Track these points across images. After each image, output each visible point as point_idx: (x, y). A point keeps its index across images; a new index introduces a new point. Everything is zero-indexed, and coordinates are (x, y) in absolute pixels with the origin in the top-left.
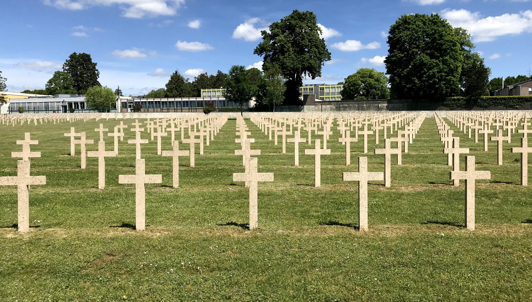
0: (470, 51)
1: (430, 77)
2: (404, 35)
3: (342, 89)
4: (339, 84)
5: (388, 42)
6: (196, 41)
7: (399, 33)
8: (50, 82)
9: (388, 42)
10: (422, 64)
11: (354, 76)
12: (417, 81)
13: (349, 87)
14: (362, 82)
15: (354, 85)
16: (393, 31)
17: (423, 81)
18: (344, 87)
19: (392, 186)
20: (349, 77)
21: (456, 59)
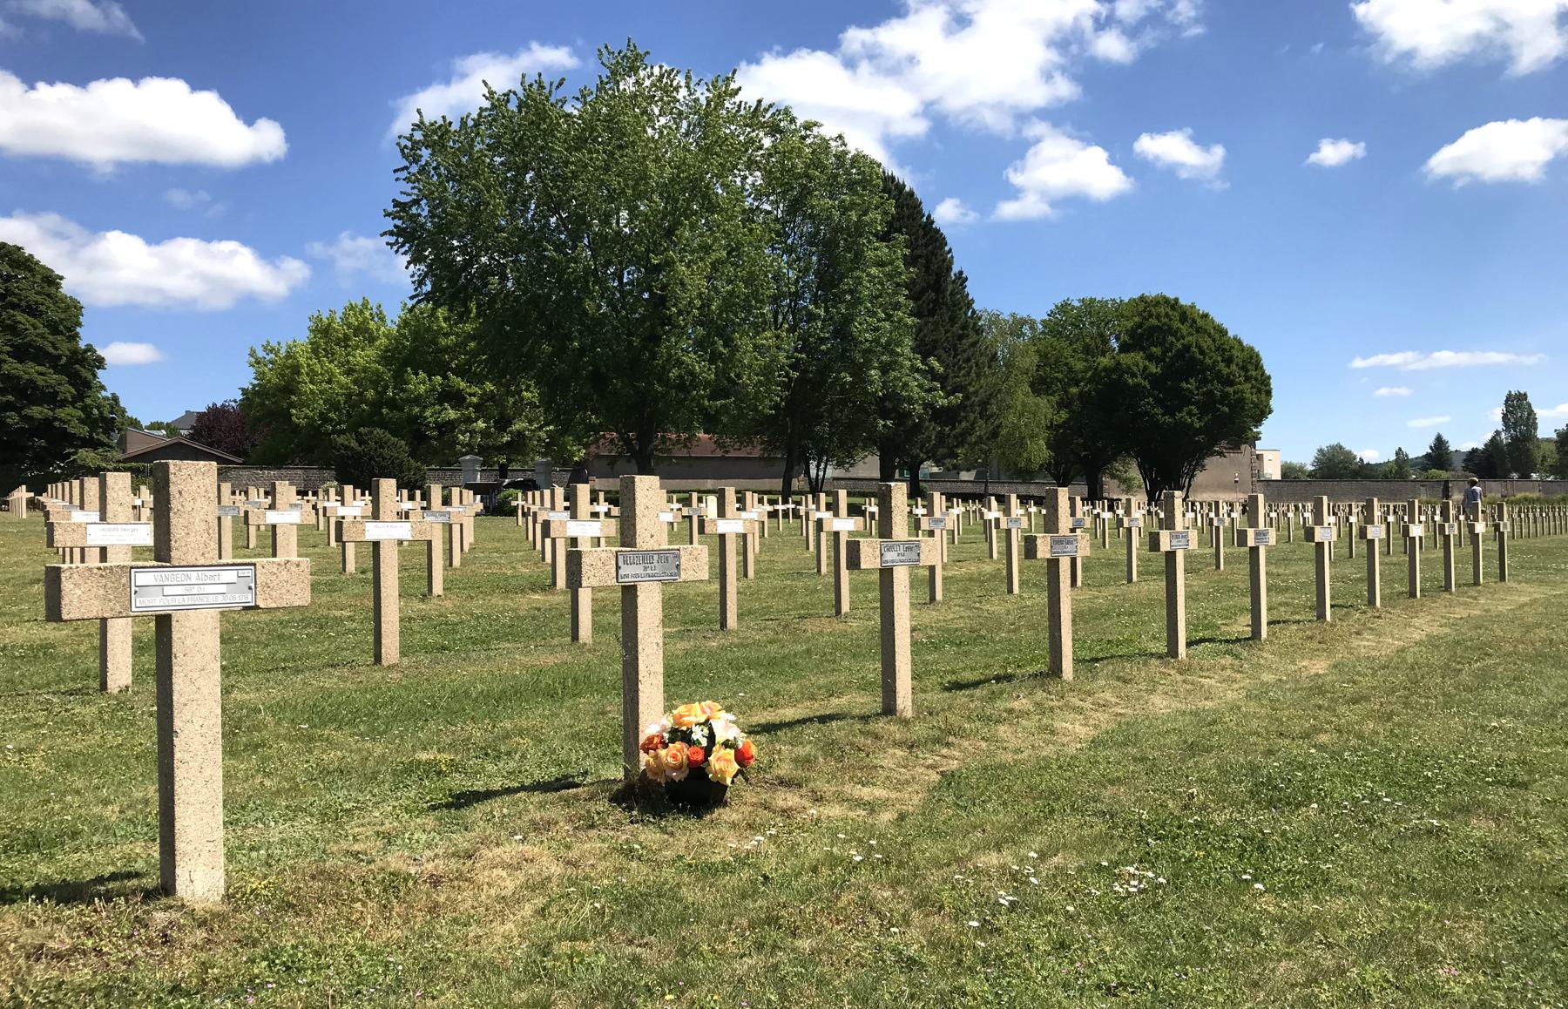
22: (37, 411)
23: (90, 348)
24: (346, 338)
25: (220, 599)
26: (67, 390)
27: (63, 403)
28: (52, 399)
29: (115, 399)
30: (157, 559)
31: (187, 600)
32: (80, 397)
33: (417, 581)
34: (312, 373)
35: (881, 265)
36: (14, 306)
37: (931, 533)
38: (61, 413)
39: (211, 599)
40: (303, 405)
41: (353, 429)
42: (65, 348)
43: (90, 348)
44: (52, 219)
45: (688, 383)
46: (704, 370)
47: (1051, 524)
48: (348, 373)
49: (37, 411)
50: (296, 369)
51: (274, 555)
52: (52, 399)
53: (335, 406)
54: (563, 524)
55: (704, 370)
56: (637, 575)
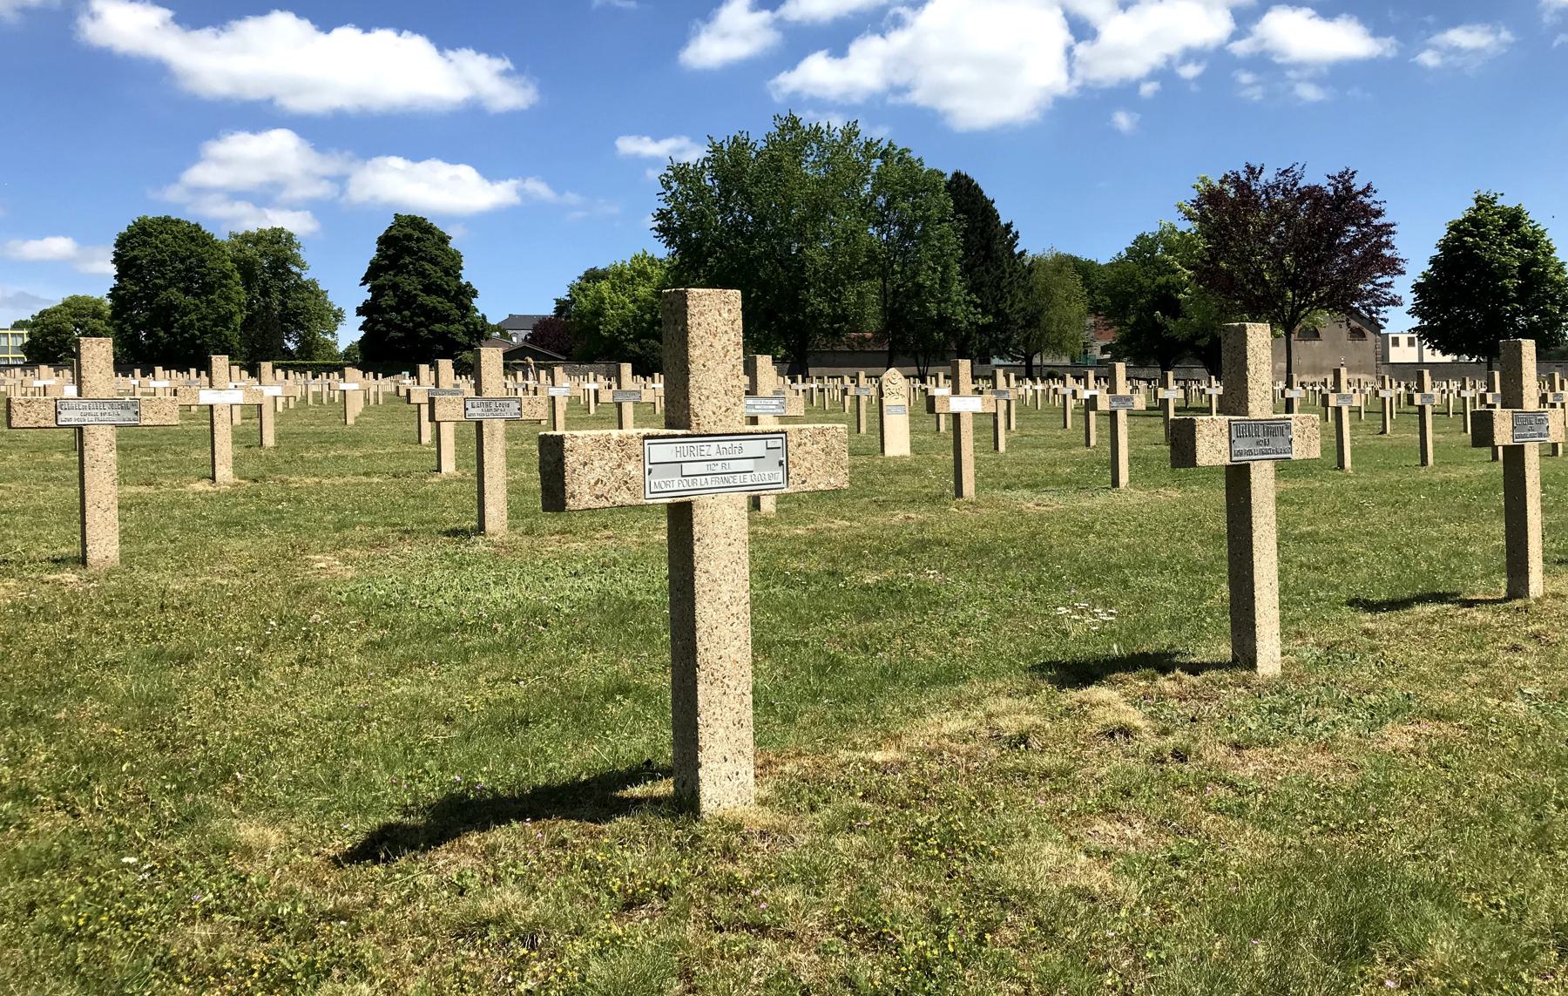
0: (299, 276)
1: (184, 328)
2: (143, 254)
3: (26, 339)
4: (17, 326)
5: (114, 262)
6: (698, 779)
7: (133, 249)
8: (1190, 55)
9: (114, 262)
10: (171, 307)
11: (55, 311)
12: (162, 334)
13: (782, 135)
14: (77, 325)
15: (57, 332)
16: (122, 242)
17: (172, 335)
18: (30, 335)
19: (126, 558)
20: (42, 314)
21: (228, 299)
22: (438, 327)
23: (468, 284)
24: (633, 278)
25: (748, 479)
26: (456, 313)
27: (453, 323)
28: (445, 319)
29: (484, 317)
30: (669, 425)
31: (711, 482)
32: (464, 316)
33: (248, 439)
34: (613, 304)
35: (950, 236)
36: (422, 259)
37: (1553, 406)
38: (452, 328)
39: (738, 480)
40: (606, 324)
41: (636, 340)
42: (453, 284)
43: (468, 284)
44: (500, 64)
45: (816, 316)
46: (825, 307)
47: (1512, 398)
48: (634, 302)
49: (438, 327)
50: (602, 300)
51: (621, 427)
52: (445, 319)
53: (626, 324)
54: (946, 399)
55: (825, 307)
56: (1250, 453)
